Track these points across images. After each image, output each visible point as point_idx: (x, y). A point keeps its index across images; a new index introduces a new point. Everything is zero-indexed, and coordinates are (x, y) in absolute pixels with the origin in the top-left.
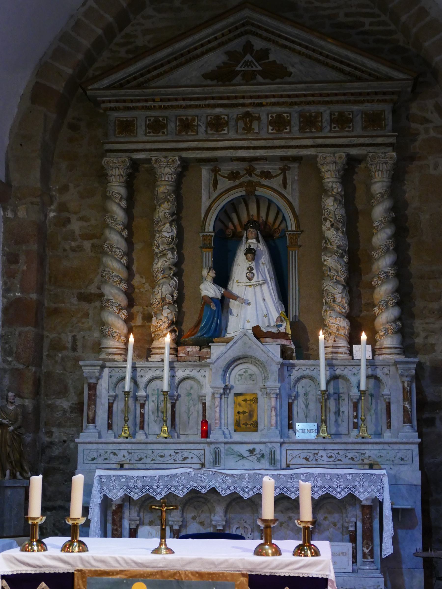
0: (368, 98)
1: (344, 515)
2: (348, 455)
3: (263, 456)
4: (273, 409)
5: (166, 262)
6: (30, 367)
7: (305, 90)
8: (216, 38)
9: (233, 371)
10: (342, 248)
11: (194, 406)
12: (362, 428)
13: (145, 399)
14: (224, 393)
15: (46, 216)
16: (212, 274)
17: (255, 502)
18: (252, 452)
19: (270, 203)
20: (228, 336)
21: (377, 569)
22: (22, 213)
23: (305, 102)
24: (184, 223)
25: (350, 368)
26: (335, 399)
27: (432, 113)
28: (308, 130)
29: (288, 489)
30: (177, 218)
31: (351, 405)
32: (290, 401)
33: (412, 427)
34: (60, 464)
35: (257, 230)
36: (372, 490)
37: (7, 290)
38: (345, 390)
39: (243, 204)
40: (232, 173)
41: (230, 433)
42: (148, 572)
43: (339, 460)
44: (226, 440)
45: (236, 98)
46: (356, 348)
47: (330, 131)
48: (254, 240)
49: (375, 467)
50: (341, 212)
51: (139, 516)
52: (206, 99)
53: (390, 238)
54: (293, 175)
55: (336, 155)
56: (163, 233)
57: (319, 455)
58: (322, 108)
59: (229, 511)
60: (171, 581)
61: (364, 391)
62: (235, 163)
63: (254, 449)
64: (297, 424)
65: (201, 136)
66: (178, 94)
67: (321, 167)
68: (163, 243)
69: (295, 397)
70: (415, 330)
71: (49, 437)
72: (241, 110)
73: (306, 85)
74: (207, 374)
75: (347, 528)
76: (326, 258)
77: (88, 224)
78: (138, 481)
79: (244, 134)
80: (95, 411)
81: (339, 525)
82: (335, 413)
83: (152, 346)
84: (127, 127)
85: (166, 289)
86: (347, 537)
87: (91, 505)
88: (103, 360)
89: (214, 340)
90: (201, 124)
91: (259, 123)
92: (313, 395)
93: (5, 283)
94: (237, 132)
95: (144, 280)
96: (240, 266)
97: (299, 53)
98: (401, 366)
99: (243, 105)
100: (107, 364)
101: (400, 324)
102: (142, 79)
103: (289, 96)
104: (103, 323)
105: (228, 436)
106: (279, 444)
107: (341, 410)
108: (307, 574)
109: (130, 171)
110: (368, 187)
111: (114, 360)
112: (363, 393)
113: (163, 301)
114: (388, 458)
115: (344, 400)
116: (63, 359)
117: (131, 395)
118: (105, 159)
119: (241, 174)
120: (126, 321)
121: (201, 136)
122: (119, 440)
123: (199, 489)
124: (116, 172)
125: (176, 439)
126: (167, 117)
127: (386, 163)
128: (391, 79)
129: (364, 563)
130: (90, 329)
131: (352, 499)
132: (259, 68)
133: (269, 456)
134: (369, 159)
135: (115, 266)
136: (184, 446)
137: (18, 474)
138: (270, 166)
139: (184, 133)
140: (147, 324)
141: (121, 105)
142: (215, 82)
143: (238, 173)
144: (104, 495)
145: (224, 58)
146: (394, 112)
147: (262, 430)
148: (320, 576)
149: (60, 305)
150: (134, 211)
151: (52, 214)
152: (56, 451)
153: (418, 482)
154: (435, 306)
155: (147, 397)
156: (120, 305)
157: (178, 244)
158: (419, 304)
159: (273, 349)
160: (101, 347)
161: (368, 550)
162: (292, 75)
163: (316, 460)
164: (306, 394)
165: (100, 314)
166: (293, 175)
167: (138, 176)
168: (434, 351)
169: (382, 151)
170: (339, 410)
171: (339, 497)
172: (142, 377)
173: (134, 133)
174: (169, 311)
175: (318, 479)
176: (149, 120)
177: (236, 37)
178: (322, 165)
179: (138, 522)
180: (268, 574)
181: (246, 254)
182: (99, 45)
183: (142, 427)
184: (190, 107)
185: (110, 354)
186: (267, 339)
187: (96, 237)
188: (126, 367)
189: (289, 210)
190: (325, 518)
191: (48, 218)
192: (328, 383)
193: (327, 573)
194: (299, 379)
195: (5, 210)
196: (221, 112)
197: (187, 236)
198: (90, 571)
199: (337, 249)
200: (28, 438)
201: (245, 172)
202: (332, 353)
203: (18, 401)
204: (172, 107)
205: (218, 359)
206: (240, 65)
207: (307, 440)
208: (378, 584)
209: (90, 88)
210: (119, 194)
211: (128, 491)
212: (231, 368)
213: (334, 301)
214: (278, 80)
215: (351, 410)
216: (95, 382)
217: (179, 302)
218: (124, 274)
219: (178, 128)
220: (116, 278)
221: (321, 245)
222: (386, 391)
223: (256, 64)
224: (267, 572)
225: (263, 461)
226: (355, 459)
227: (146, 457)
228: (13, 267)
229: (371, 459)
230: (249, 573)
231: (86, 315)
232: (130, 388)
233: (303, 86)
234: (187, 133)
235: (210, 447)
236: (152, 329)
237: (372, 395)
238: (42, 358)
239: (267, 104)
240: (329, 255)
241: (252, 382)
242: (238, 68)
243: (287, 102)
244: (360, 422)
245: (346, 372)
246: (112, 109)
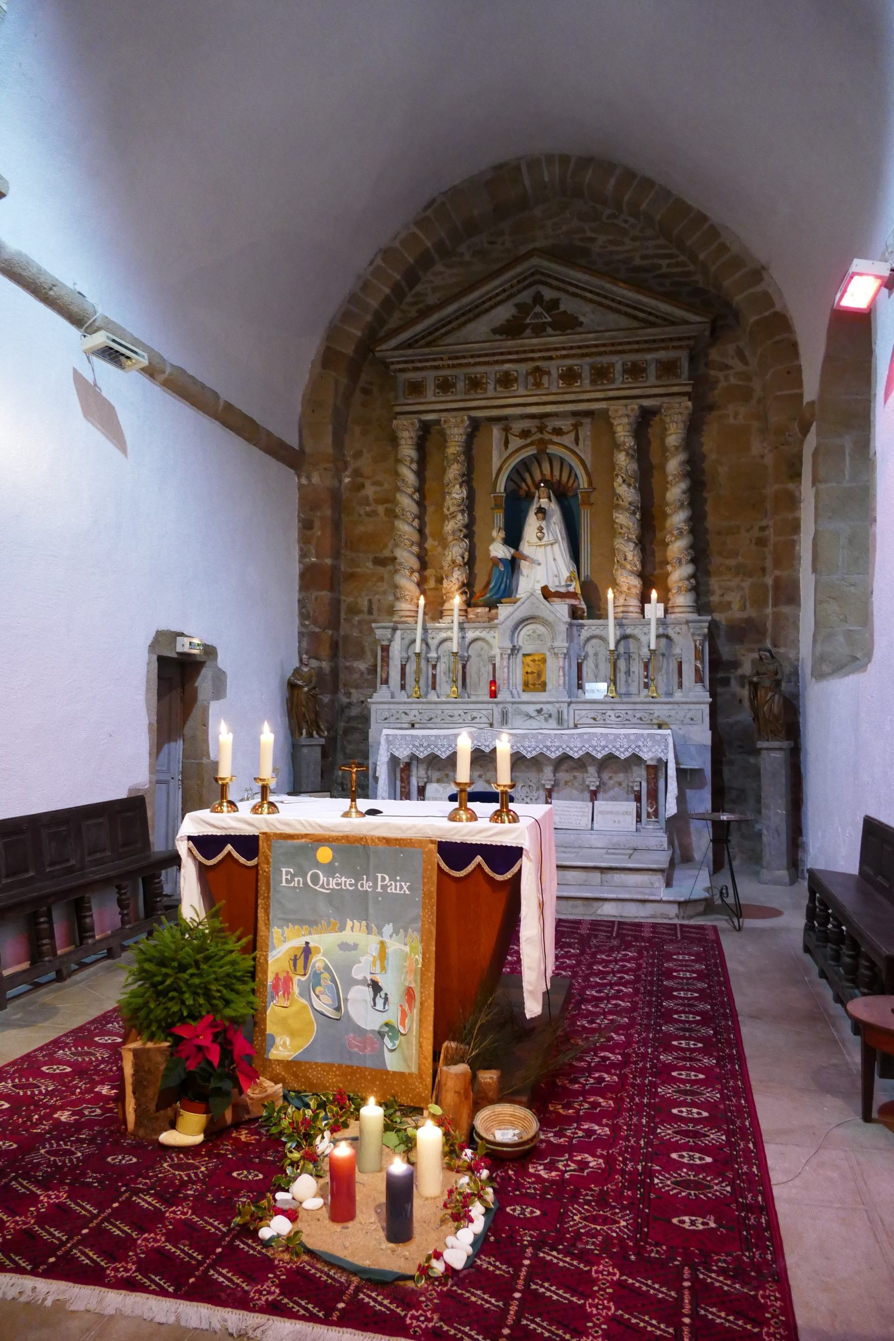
0: (663, 345)
3: (550, 716)
7: (596, 340)
8: (504, 291)
11: (485, 666)
15: (340, 482)
16: (502, 534)
17: (452, 760)
18: (539, 711)
20: (518, 596)
22: (316, 479)
24: (475, 484)
25: (641, 627)
30: (468, 479)
31: (642, 665)
33: (704, 686)
37: (303, 555)
40: (523, 431)
45: (525, 352)
46: (647, 606)
47: (623, 383)
48: (546, 500)
49: (664, 727)
50: (634, 466)
51: (426, 773)
52: (494, 355)
53: (684, 492)
54: (586, 431)
58: (614, 358)
63: (541, 709)
65: (490, 393)
66: (467, 351)
70: (711, 588)
72: (530, 365)
74: (496, 635)
75: (632, 787)
81: (624, 785)
82: (626, 673)
85: (456, 551)
86: (632, 796)
88: (395, 622)
89: (503, 600)
93: (301, 549)
95: (436, 543)
96: (532, 524)
97: (591, 301)
99: (532, 359)
100: (399, 626)
102: (429, 338)
103: (579, 347)
104: (396, 587)
107: (632, 669)
111: (405, 622)
112: (652, 652)
116: (359, 622)
117: (423, 656)
118: (394, 421)
120: (419, 584)
121: (490, 393)
122: (410, 700)
123: (482, 748)
124: (406, 434)
125: (467, 699)
128: (686, 322)
129: (648, 823)
131: (636, 759)
132: (549, 319)
134: (663, 410)
135: (406, 529)
136: (472, 706)
137: (315, 733)
138: (562, 423)
141: (410, 366)
142: (504, 337)
146: (692, 359)
148: (514, 845)
149: (355, 570)
151: (347, 480)
152: (354, 712)
154: (732, 562)
155: (438, 658)
156: (411, 568)
157: (469, 505)
158: (716, 560)
159: (561, 609)
164: (596, 654)
167: (428, 437)
171: (622, 757)
174: (459, 573)
177: (525, 288)
179: (425, 780)
181: (536, 514)
182: (388, 305)
183: (434, 688)
184: (479, 364)
186: (555, 599)
187: (389, 501)
189: (581, 468)
192: (617, 643)
193: (522, 842)
195: (299, 477)
198: (275, 834)
200: (326, 699)
202: (623, 612)
203: (314, 663)
204: (461, 365)
213: (625, 559)
214: (569, 331)
217: (470, 564)
218: (415, 537)
222: (677, 651)
224: (458, 839)
225: (550, 721)
228: (308, 532)
231: (382, 579)
232: (421, 650)
234: (476, 392)
236: (444, 592)
237: (663, 655)
238: (339, 622)
239: (557, 357)
240: (620, 512)
241: (540, 642)
242: (528, 321)
245: (636, 632)
246: (402, 370)
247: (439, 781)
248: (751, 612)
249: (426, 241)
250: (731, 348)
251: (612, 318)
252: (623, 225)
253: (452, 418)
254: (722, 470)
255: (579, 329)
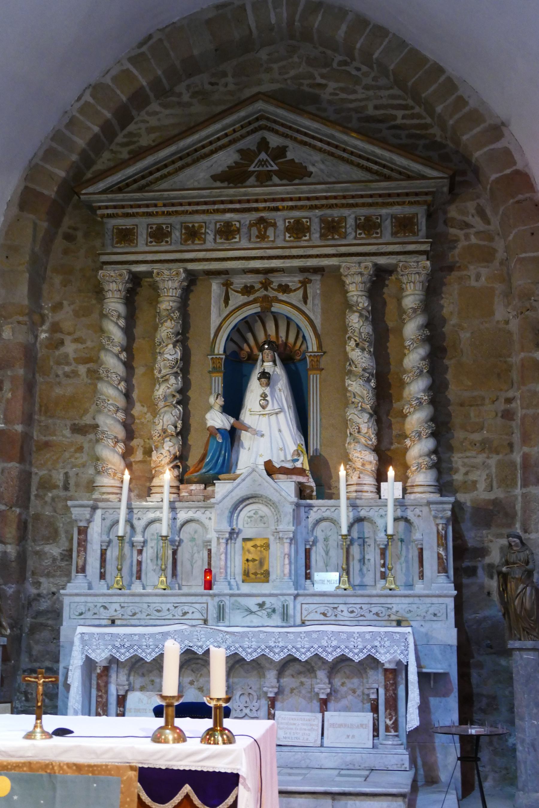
1: (365, 681)
2: (372, 609)
3: (274, 611)
4: (287, 556)
5: (169, 388)
6: (13, 509)
7: (327, 191)
8: (226, 135)
9: (242, 513)
10: (369, 371)
11: (199, 552)
12: (388, 579)
13: (142, 544)
14: (230, 538)
15: (36, 337)
16: (221, 401)
18: (261, 605)
19: (289, 321)
20: (238, 472)
21: (402, 744)
23: (327, 205)
24: (191, 344)
26: (360, 545)
27: (473, 216)
28: (330, 237)
29: (298, 650)
30: (182, 338)
31: (378, 551)
32: (308, 547)
33: (448, 577)
34: (48, 619)
35: (274, 351)
36: (395, 651)
38: (371, 535)
39: (259, 323)
40: (246, 287)
41: (237, 585)
42: (13, 763)
43: (361, 616)
44: (231, 592)
45: (248, 201)
46: (383, 485)
47: (355, 238)
48: (271, 363)
49: (403, 624)
50: (367, 329)
51: (128, 680)
52: (214, 203)
53: (423, 359)
54: (315, 288)
55: (362, 265)
56: (166, 356)
57: (339, 609)
58: (345, 212)
59: (232, 675)
60: (42, 775)
61: (392, 535)
62: (250, 276)
64: (316, 574)
65: (210, 244)
66: (183, 197)
67: (344, 278)
68: (165, 367)
69: (313, 542)
71: (37, 588)
72: (255, 216)
73: (327, 186)
74: (213, 516)
75: (368, 695)
76: (350, 382)
77: (84, 346)
78: (125, 640)
79: (257, 242)
80: (85, 558)
81: (359, 692)
82: (360, 561)
83: (152, 485)
84: (126, 236)
85: (168, 419)
86: (368, 706)
87: (70, 668)
88: (96, 500)
89: (221, 476)
90: (210, 232)
91: (275, 229)
92: (335, 540)
94: (250, 240)
95: (145, 409)
96: (254, 390)
97: (320, 150)
98: (434, 506)
99: (257, 210)
100: (100, 504)
101: (435, 458)
102: (143, 182)
103: (308, 199)
105: (235, 587)
106: (292, 597)
107: (367, 557)
108: (213, 768)
109: (129, 285)
110: (399, 300)
111: (108, 500)
112: (390, 537)
113: (164, 433)
114: (419, 614)
115: (369, 545)
116: (53, 499)
118: (100, 272)
119: (256, 289)
121: (210, 244)
122: (110, 591)
123: (195, 649)
124: (113, 286)
125: (177, 591)
126: (171, 225)
127: (418, 273)
128: (424, 177)
130: (84, 465)
131: (371, 662)
132: (275, 168)
133: (281, 610)
134: (399, 269)
135: (111, 393)
136: (183, 599)
139: (190, 242)
140: (148, 459)
141: (120, 211)
142: (225, 184)
143: (252, 287)
144: (86, 656)
145: (236, 157)
146: (429, 216)
147: (274, 580)
148: (229, 771)
150: (135, 331)
151: (43, 336)
152: (44, 605)
153: (454, 641)
154: (476, 437)
155: (145, 542)
156: (115, 437)
157: (184, 367)
158: (459, 435)
159: (287, 487)
160: (95, 485)
161: (391, 722)
162: (313, 175)
163: (336, 616)
164: (326, 540)
165: (93, 448)
166: (315, 288)
167: (138, 290)
168: (476, 489)
169: (415, 259)
170: (364, 558)
171: (357, 659)
172: (139, 519)
173: (134, 243)
174: (171, 444)
175: (332, 639)
176: (151, 228)
177: (249, 134)
178: (346, 276)
179: (127, 687)
180: (164, 768)
181: (259, 379)
182: (97, 145)
183: (139, 578)
185: (104, 493)
186: (281, 476)
187: (91, 360)
188: (119, 508)
189: (310, 328)
190: (343, 684)
191: (39, 340)
192: (350, 527)
193: (238, 767)
194: (318, 522)
196: (231, 218)
197: (196, 358)
199: (363, 372)
201: (260, 286)
202: (356, 491)
204: (177, 213)
205: (224, 499)
206: (253, 165)
207: (325, 592)
208: (402, 763)
209: (83, 192)
210: (115, 311)
211: (114, 651)
212: (239, 509)
213: (359, 432)
214: (297, 181)
215: (378, 557)
216: (86, 525)
217: (183, 433)
218: (121, 402)
219: (183, 237)
220: (111, 407)
221: (345, 368)
222: (417, 536)
223: (272, 163)
224: (162, 765)
226: (381, 615)
227: (141, 611)
229: (398, 614)
230: (141, 766)
231: (80, 449)
233: (323, 186)
234: (193, 242)
235: (213, 600)
236: (153, 465)
237: (402, 541)
238: (29, 499)
239: (284, 209)
240: (353, 379)
241: (263, 525)
242: (251, 168)
243: (306, 206)
244: (388, 571)
246: (110, 216)
247: (142, 689)
248: (498, 493)
249: (140, 78)
250: (471, 206)
251: (345, 170)
252: (354, 72)
253: (165, 270)
254: (465, 336)
255: (307, 180)
